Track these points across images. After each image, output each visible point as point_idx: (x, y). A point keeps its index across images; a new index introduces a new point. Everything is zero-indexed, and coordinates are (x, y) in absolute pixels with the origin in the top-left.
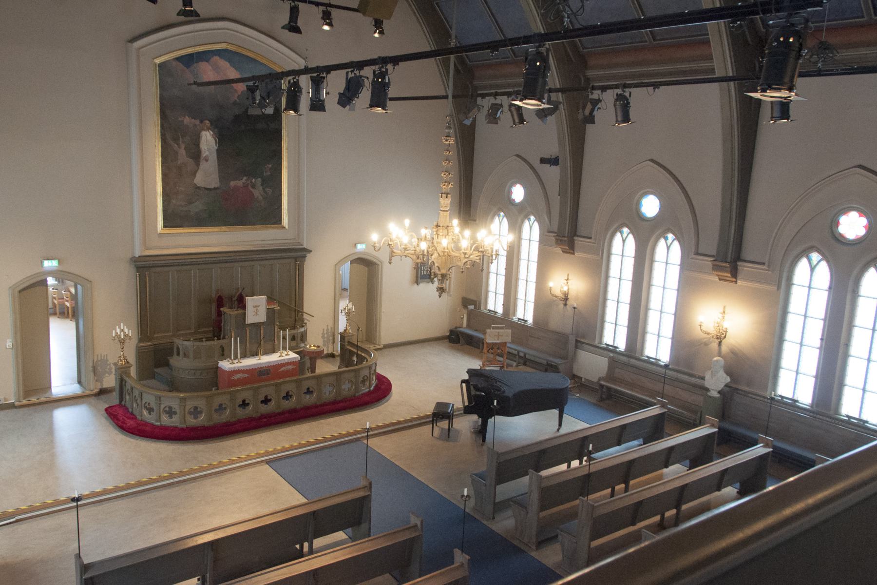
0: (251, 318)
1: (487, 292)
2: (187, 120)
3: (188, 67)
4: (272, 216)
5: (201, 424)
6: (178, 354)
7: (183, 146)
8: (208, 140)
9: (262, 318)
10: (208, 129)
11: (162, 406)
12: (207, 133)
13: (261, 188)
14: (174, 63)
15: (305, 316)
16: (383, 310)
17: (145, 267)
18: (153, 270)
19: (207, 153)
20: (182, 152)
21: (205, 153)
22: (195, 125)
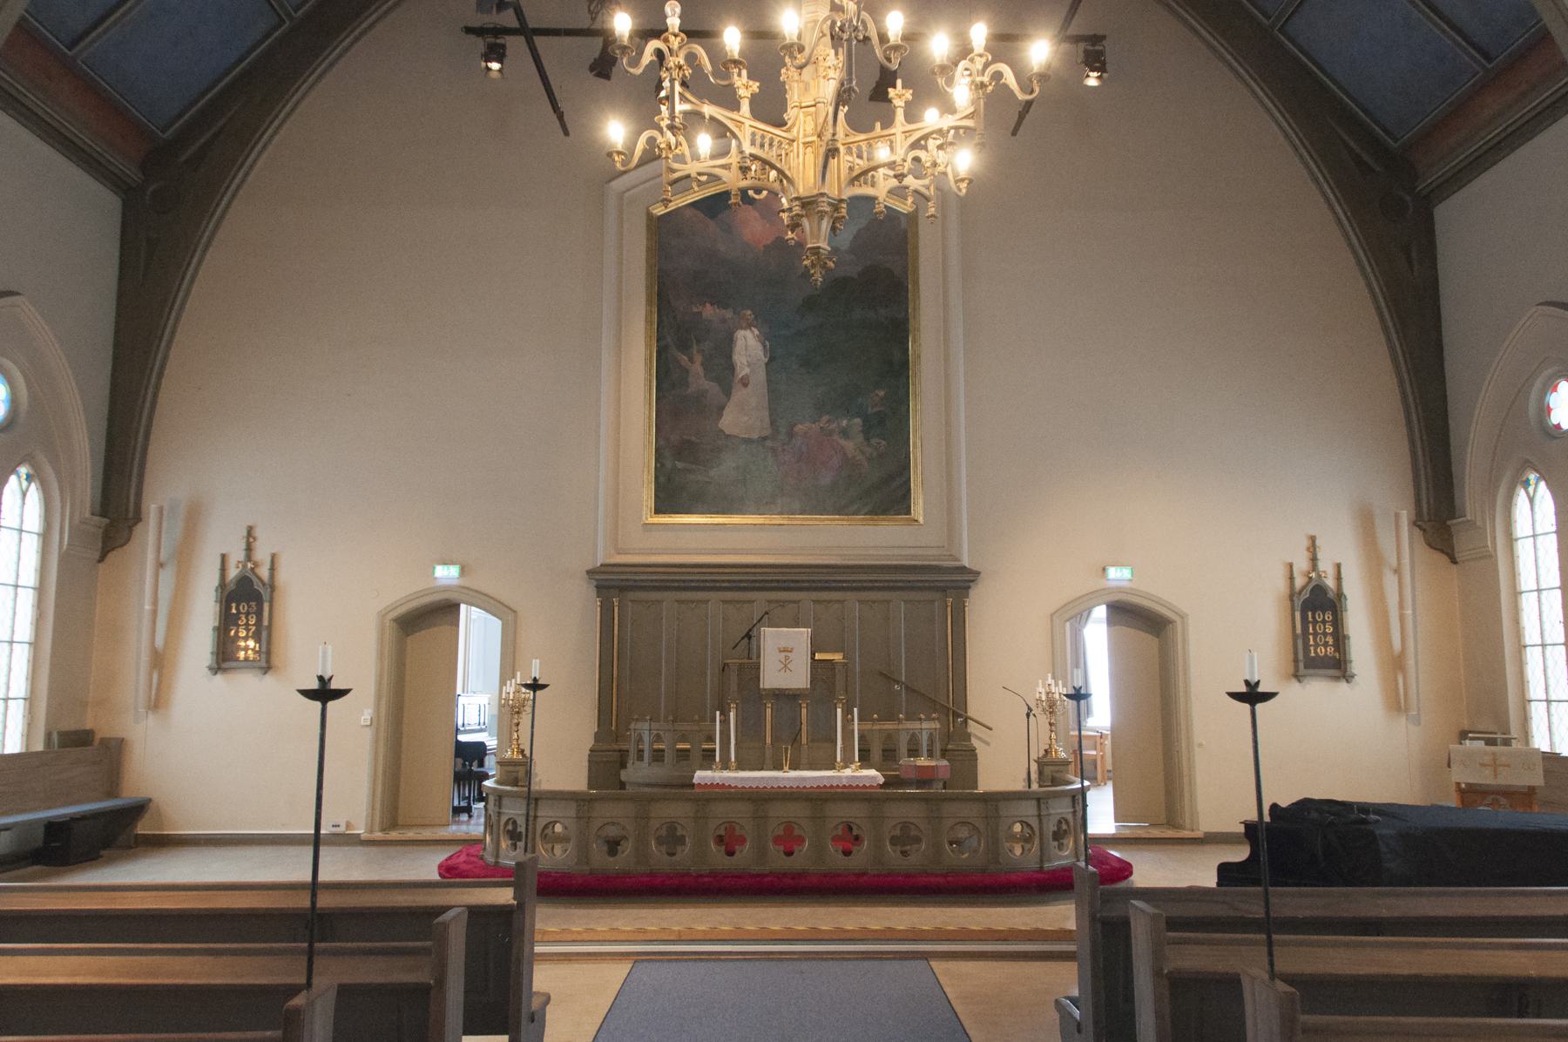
0: (773, 676)
1: (1525, 703)
2: (709, 311)
3: (712, 217)
4: (888, 493)
6: (640, 757)
7: (698, 359)
8: (749, 347)
9: (798, 677)
10: (749, 326)
11: (504, 819)
12: (748, 333)
13: (860, 438)
14: (689, 213)
15: (973, 728)
16: (1198, 737)
17: (616, 586)
18: (631, 595)
19: (747, 371)
20: (697, 368)
21: (742, 370)
22: (724, 321)
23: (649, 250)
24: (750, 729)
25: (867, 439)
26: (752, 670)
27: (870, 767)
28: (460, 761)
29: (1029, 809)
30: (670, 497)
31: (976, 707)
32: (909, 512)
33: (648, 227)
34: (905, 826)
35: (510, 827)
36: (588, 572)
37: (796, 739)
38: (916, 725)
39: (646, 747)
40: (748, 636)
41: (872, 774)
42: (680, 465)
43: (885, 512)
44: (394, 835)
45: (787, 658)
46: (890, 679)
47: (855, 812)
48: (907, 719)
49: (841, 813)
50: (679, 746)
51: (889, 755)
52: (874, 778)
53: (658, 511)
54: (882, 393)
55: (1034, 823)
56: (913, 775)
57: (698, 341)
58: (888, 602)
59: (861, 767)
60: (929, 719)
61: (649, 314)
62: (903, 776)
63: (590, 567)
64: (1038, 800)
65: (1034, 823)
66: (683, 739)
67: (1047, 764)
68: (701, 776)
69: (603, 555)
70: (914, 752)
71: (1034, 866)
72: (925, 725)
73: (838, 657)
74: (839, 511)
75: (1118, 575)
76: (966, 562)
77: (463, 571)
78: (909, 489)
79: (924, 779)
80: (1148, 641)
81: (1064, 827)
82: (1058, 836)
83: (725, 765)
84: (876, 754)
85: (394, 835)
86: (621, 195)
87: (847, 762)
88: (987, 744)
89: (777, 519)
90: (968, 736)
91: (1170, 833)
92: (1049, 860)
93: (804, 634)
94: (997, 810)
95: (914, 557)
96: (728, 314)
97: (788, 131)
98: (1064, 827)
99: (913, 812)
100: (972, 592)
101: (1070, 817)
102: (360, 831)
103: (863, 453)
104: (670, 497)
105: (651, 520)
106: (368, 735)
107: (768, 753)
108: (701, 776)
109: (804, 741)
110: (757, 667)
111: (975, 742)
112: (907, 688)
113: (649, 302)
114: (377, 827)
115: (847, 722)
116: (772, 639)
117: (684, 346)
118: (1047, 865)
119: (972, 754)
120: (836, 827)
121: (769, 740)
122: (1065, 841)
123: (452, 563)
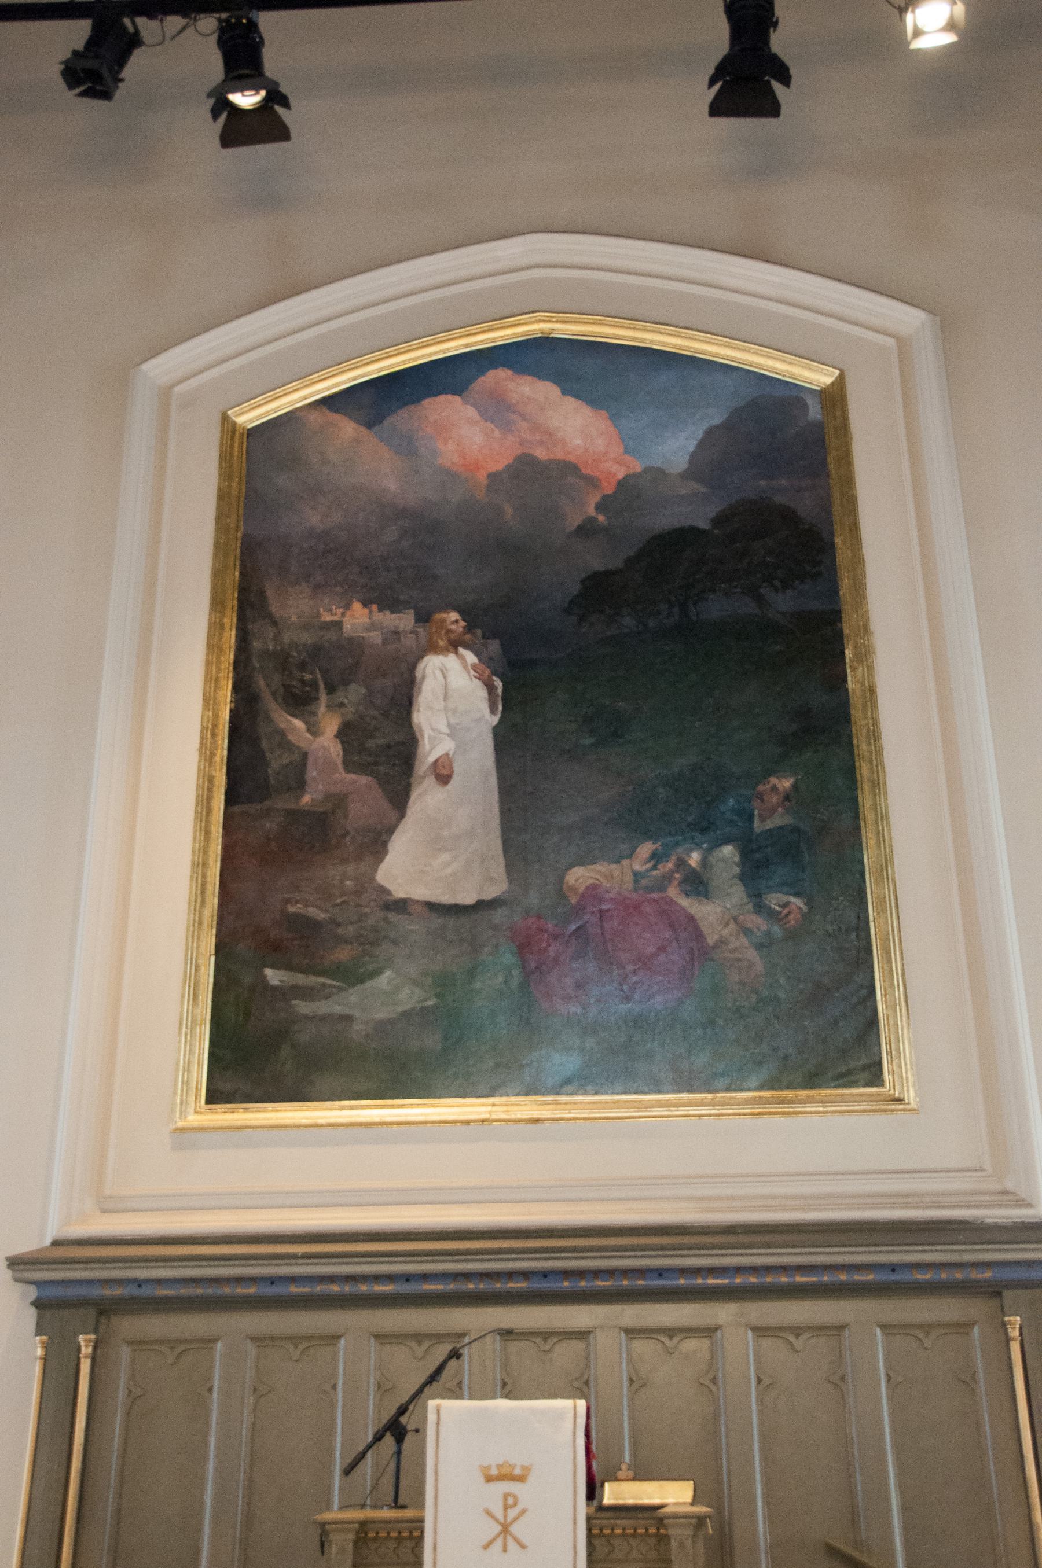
4: (826, 1032)
8: (453, 698)
10: (454, 645)
12: (450, 661)
13: (738, 893)
17: (94, 1299)
23: (223, 496)
25: (756, 896)
28: (621, 1474)
30: (257, 1051)
32: (875, 1077)
33: (225, 458)
36: (15, 1263)
42: (273, 976)
43: (812, 1080)
45: (509, 1502)
53: (214, 1097)
54: (786, 784)
57: (331, 690)
61: (215, 629)
69: (60, 1213)
73: (674, 1495)
78: (873, 1022)
86: (165, 394)
89: (504, 1099)
96: (405, 621)
97: (908, 1104)
103: (747, 931)
104: (257, 1051)
105: (193, 1119)
113: (217, 603)
116: (465, 1436)
117: (299, 701)
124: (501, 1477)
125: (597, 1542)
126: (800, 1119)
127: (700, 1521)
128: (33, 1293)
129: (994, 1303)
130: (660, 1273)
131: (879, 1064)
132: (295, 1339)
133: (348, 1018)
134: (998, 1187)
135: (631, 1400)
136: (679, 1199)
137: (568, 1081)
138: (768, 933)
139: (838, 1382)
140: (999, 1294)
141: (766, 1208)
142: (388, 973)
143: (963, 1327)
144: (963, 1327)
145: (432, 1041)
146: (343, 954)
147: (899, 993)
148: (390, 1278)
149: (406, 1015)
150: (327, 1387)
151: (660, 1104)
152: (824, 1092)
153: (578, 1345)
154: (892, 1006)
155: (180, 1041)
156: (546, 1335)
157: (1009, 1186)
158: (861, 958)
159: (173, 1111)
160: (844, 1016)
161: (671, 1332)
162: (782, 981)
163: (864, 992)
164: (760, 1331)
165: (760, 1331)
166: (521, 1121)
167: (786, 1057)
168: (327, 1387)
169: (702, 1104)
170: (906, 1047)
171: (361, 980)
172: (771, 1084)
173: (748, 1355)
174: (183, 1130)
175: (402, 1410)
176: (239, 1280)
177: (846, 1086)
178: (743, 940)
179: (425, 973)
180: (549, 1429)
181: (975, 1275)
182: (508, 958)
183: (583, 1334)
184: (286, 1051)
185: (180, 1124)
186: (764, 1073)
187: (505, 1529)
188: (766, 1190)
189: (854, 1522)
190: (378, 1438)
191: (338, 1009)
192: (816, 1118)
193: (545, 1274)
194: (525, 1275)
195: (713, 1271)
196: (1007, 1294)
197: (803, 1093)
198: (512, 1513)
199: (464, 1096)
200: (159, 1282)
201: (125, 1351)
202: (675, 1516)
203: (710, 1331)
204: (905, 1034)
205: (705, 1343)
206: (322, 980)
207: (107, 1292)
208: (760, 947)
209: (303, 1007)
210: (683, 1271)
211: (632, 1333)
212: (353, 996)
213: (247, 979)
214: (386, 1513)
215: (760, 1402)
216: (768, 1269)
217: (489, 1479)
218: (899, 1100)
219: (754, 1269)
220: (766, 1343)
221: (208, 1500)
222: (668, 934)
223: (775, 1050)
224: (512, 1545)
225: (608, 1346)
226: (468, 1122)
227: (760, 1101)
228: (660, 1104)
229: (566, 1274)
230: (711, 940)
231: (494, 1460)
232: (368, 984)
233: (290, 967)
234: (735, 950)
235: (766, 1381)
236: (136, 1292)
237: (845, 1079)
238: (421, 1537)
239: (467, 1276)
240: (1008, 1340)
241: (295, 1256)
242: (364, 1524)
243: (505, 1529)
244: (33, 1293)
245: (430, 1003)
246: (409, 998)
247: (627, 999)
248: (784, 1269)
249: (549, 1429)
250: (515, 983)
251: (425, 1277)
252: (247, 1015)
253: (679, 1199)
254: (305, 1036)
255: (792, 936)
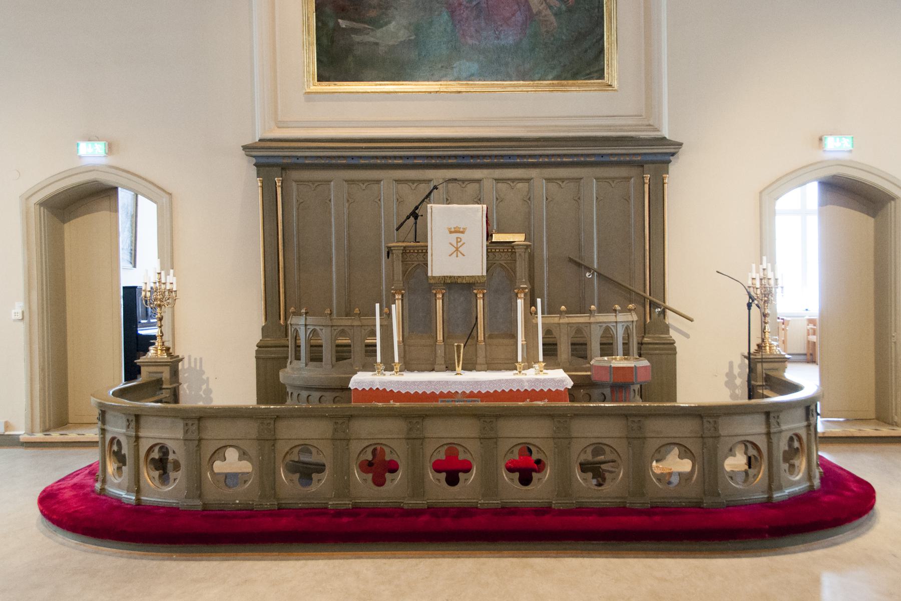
4: (578, 52)
5: (316, 503)
9: (472, 263)
15: (671, 319)
17: (276, 163)
18: (296, 175)
24: (418, 322)
26: (415, 256)
27: (556, 366)
29: (754, 428)
31: (677, 292)
32: (601, 77)
34: (598, 449)
35: (115, 448)
36: (245, 148)
37: (471, 335)
38: (609, 318)
39: (302, 342)
40: (414, 215)
41: (559, 378)
42: (343, 23)
43: (575, 76)
44: (55, 436)
45: (458, 240)
46: (579, 265)
47: (535, 433)
48: (600, 310)
49: (516, 433)
50: (339, 342)
51: (580, 350)
52: (561, 381)
55: (762, 443)
56: (607, 378)
58: (578, 180)
59: (547, 367)
60: (625, 310)
62: (596, 378)
63: (248, 141)
64: (767, 414)
65: (762, 443)
66: (343, 333)
67: (762, 361)
68: (361, 380)
69: (262, 129)
70: (607, 348)
71: (760, 496)
72: (621, 317)
73: (518, 238)
74: (523, 76)
75: (838, 146)
76: (666, 133)
77: (111, 148)
78: (602, 51)
79: (620, 385)
80: (864, 223)
81: (796, 444)
82: (791, 454)
83: (389, 367)
84: (564, 350)
85: (55, 436)
87: (530, 362)
88: (687, 336)
89: (455, 86)
90: (666, 329)
91: (885, 431)
92: (780, 488)
93: (478, 211)
94: (716, 429)
95: (609, 128)
98: (796, 444)
99: (607, 431)
100: (672, 168)
101: (803, 433)
102: (21, 431)
103: (550, 7)
105: (313, 88)
106: (22, 327)
107: (440, 352)
108: (361, 380)
109: (481, 337)
110: (424, 251)
111: (673, 334)
112: (599, 275)
114: (37, 426)
115: (530, 315)
116: (441, 217)
118: (777, 496)
119: (670, 347)
120: (511, 450)
121: (440, 337)
122: (796, 462)
123: (98, 139)
124: (456, 232)
125: (490, 254)
126: (568, 93)
127: (527, 246)
128: (254, 160)
129: (641, 169)
130: (510, 157)
131: (603, 69)
132: (363, 181)
133: (377, 44)
134: (647, 123)
135: (497, 206)
136: (519, 127)
137: (473, 75)
138: (560, 8)
139: (578, 199)
140: (642, 166)
141: (553, 131)
142: (393, 23)
143: (628, 179)
144: (628, 179)
145: (413, 55)
146: (373, 14)
147: (614, 38)
148: (401, 157)
149: (403, 43)
150: (377, 200)
151: (511, 86)
152: (580, 82)
153: (476, 185)
154: (610, 44)
155: (303, 52)
156: (463, 181)
157: (651, 122)
158: (599, 22)
159: (303, 84)
160: (590, 48)
161: (513, 180)
162: (565, 31)
163: (599, 37)
164: (549, 180)
165: (549, 180)
166: (451, 92)
167: (565, 66)
168: (377, 200)
169: (528, 86)
170: (615, 63)
171: (382, 27)
172: (558, 78)
173: (380, 234)
174: (309, 93)
175: (417, 208)
176: (339, 157)
177: (589, 79)
178: (549, 12)
179: (410, 24)
180: (472, 216)
181: (635, 158)
182: (445, 16)
183: (478, 181)
184: (350, 59)
185: (308, 90)
186: (555, 73)
187: (457, 249)
188: (569, 123)
189: (580, 250)
190: (408, 218)
191: (372, 39)
192: (575, 93)
193: (463, 157)
194: (456, 157)
195: (531, 156)
196: (646, 166)
197: (571, 82)
198: (459, 244)
199: (428, 80)
200: (306, 157)
201: (294, 184)
202: (518, 245)
203: (528, 180)
204: (615, 56)
205: (527, 184)
206: (363, 25)
207: (286, 161)
208: (555, 15)
209: (357, 38)
210: (519, 156)
211: (498, 180)
212: (379, 33)
213: (331, 24)
214: (412, 244)
215: (547, 207)
216: (553, 155)
217: (451, 232)
218: (610, 86)
219: (547, 156)
220: (550, 185)
221: (333, 240)
222: (516, 7)
223: (560, 62)
224: (459, 254)
225: (488, 185)
226: (430, 92)
227: (553, 85)
228: (511, 86)
229: (472, 157)
230: (535, 11)
231: (453, 226)
232: (384, 28)
233: (350, 19)
234: (545, 16)
235: (550, 199)
236: (295, 161)
237: (589, 76)
238: (427, 252)
239: (432, 157)
240: (644, 183)
241: (362, 148)
242: (405, 247)
243: (457, 249)
244: (254, 160)
245: (413, 38)
246: (403, 35)
247: (498, 38)
248: (559, 156)
249: (472, 216)
250: (449, 29)
251: (415, 157)
252: (332, 42)
253: (519, 127)
254: (359, 51)
255: (570, 10)
